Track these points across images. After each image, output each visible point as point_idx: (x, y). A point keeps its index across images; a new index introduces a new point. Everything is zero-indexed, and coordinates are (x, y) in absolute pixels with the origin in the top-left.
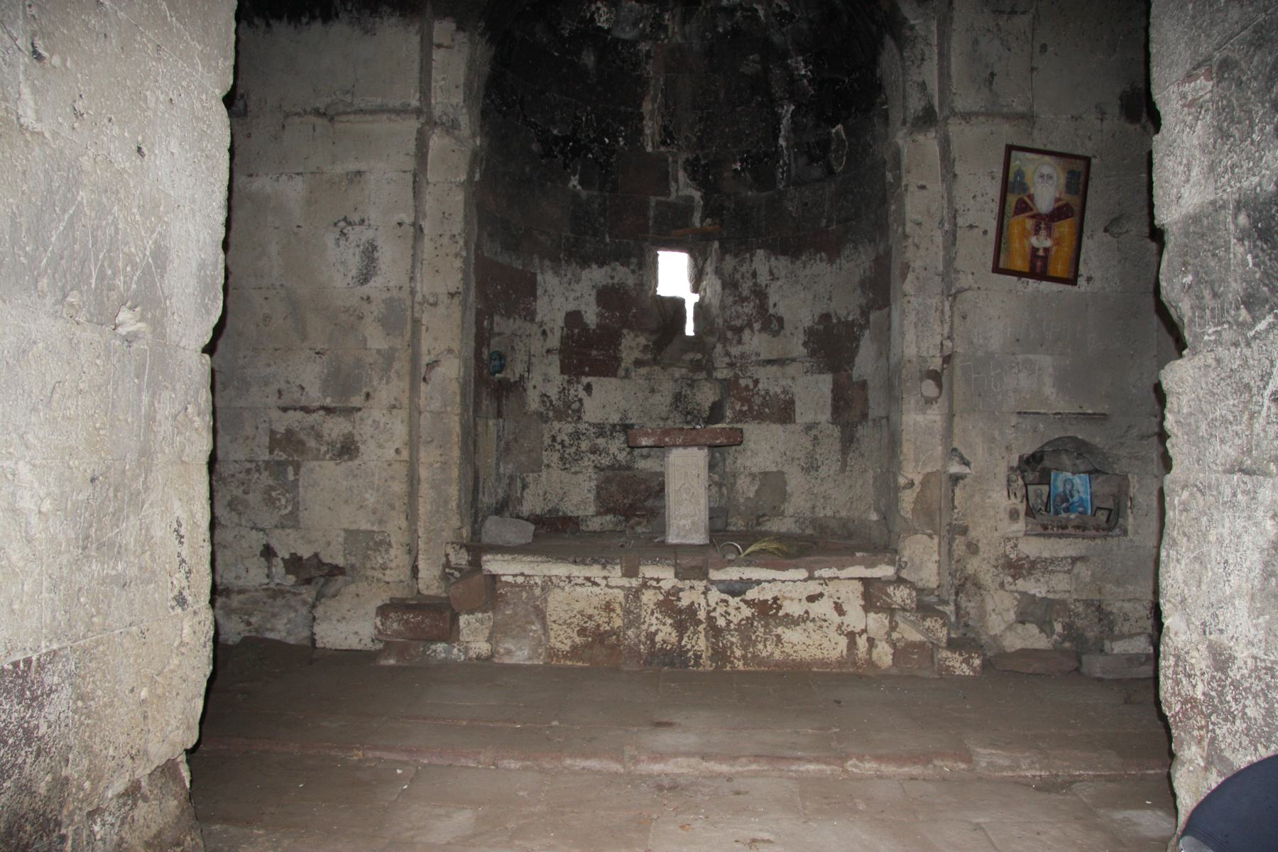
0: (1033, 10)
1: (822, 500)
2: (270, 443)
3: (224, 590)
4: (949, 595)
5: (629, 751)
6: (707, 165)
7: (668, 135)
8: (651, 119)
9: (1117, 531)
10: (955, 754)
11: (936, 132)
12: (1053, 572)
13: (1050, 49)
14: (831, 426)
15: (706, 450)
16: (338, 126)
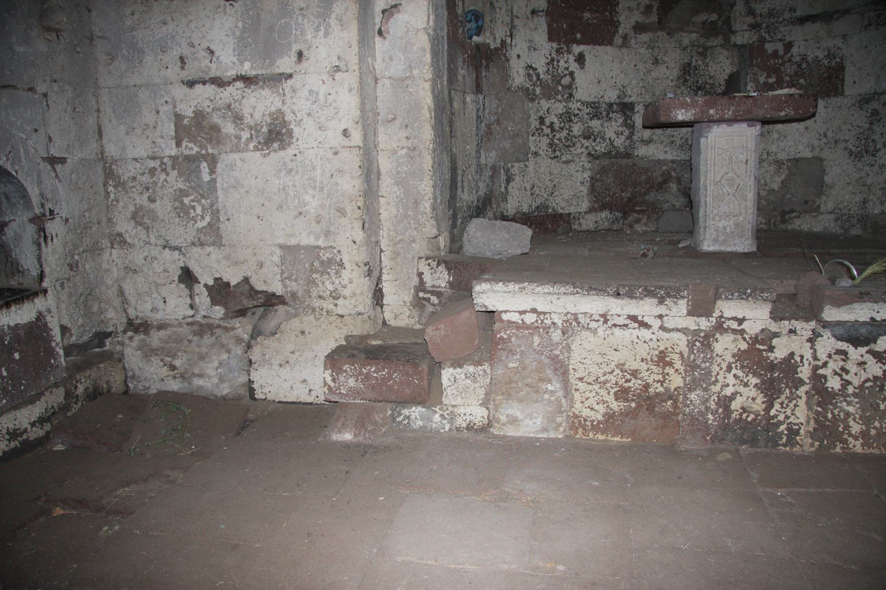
2: (176, 132)
3: (141, 325)
15: (758, 127)
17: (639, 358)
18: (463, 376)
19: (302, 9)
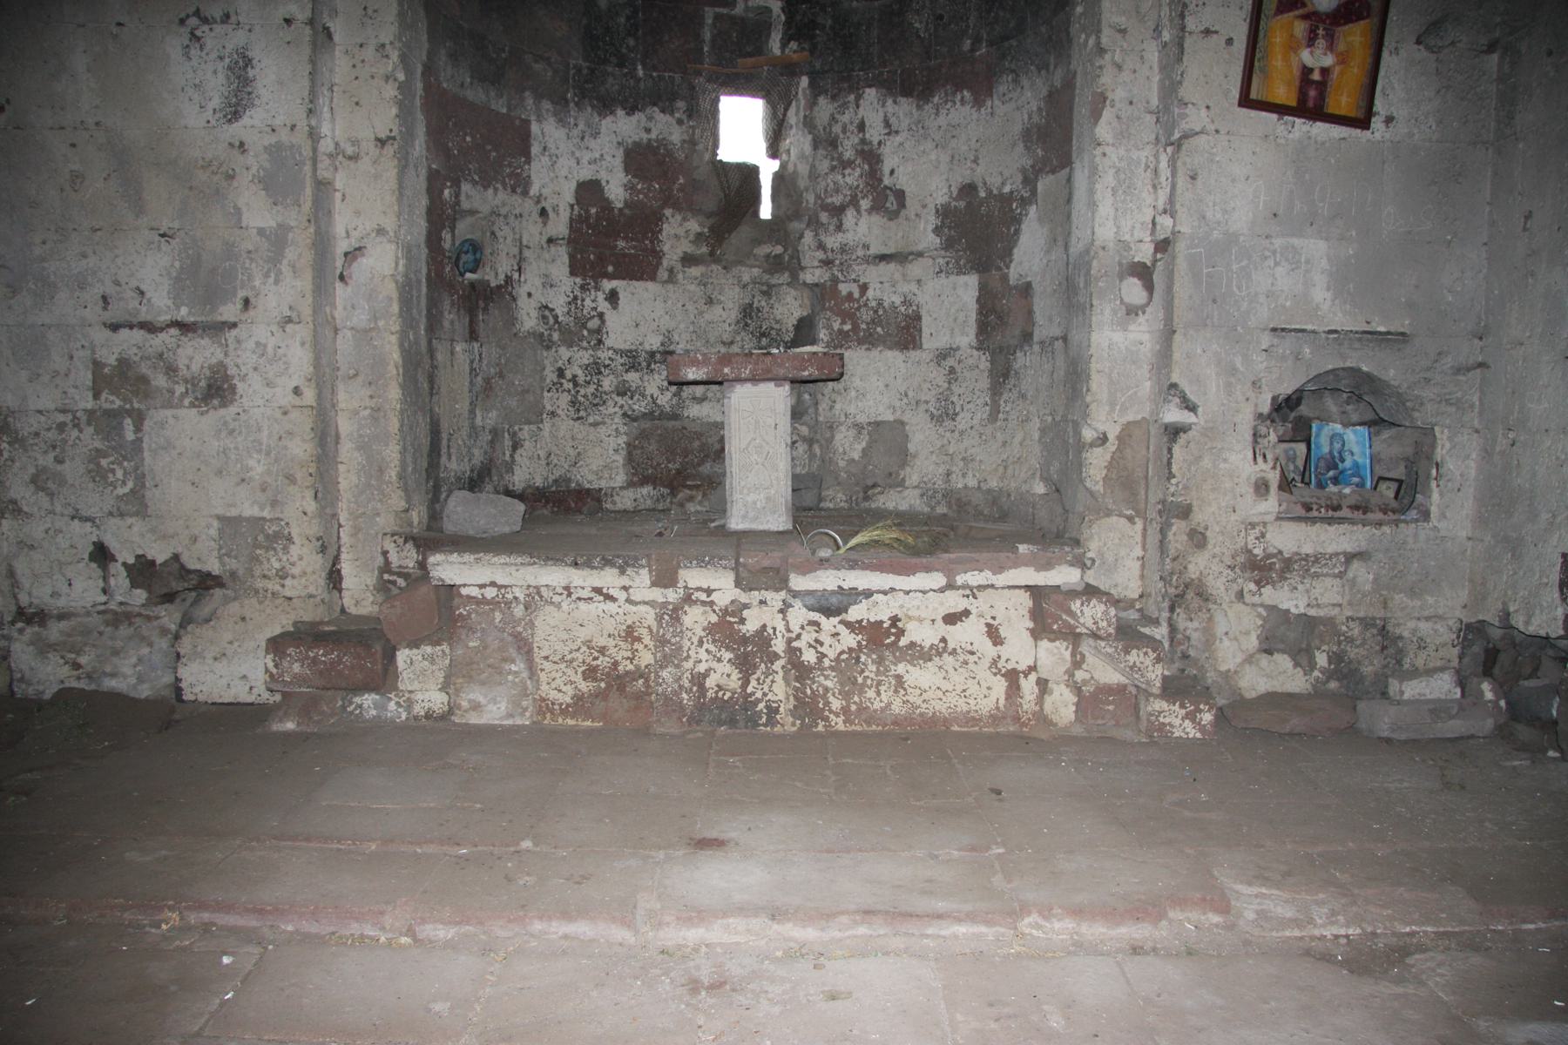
1: (961, 464)
3: (35, 614)
4: (1160, 610)
5: (646, 902)
9: (1413, 514)
10: (1204, 900)
12: (1316, 576)
14: (975, 353)
17: (605, 634)
18: (420, 658)
19: (249, 252)
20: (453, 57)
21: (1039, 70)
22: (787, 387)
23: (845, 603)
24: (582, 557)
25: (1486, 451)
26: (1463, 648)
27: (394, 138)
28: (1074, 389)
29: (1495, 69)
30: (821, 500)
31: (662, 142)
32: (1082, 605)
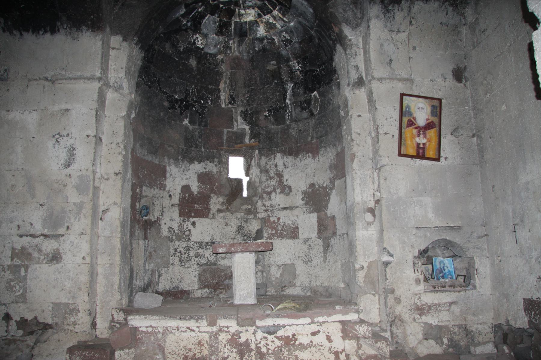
0: (408, 30)
6: (252, 113)
7: (232, 100)
8: (224, 92)
9: (470, 287)
11: (365, 88)
12: (440, 311)
13: (417, 48)
14: (317, 239)
16: (57, 86)
17: (191, 343)
18: (124, 354)
19: (70, 211)
20: (141, 146)
21: (333, 146)
22: (254, 254)
23: (276, 330)
24: (183, 316)
25: (492, 264)
26: (495, 334)
27: (121, 173)
28: (351, 251)
29: (476, 142)
30: (266, 292)
31: (210, 172)
32: (359, 327)
